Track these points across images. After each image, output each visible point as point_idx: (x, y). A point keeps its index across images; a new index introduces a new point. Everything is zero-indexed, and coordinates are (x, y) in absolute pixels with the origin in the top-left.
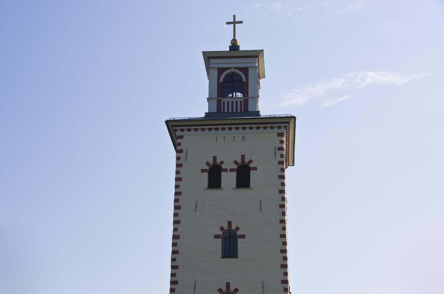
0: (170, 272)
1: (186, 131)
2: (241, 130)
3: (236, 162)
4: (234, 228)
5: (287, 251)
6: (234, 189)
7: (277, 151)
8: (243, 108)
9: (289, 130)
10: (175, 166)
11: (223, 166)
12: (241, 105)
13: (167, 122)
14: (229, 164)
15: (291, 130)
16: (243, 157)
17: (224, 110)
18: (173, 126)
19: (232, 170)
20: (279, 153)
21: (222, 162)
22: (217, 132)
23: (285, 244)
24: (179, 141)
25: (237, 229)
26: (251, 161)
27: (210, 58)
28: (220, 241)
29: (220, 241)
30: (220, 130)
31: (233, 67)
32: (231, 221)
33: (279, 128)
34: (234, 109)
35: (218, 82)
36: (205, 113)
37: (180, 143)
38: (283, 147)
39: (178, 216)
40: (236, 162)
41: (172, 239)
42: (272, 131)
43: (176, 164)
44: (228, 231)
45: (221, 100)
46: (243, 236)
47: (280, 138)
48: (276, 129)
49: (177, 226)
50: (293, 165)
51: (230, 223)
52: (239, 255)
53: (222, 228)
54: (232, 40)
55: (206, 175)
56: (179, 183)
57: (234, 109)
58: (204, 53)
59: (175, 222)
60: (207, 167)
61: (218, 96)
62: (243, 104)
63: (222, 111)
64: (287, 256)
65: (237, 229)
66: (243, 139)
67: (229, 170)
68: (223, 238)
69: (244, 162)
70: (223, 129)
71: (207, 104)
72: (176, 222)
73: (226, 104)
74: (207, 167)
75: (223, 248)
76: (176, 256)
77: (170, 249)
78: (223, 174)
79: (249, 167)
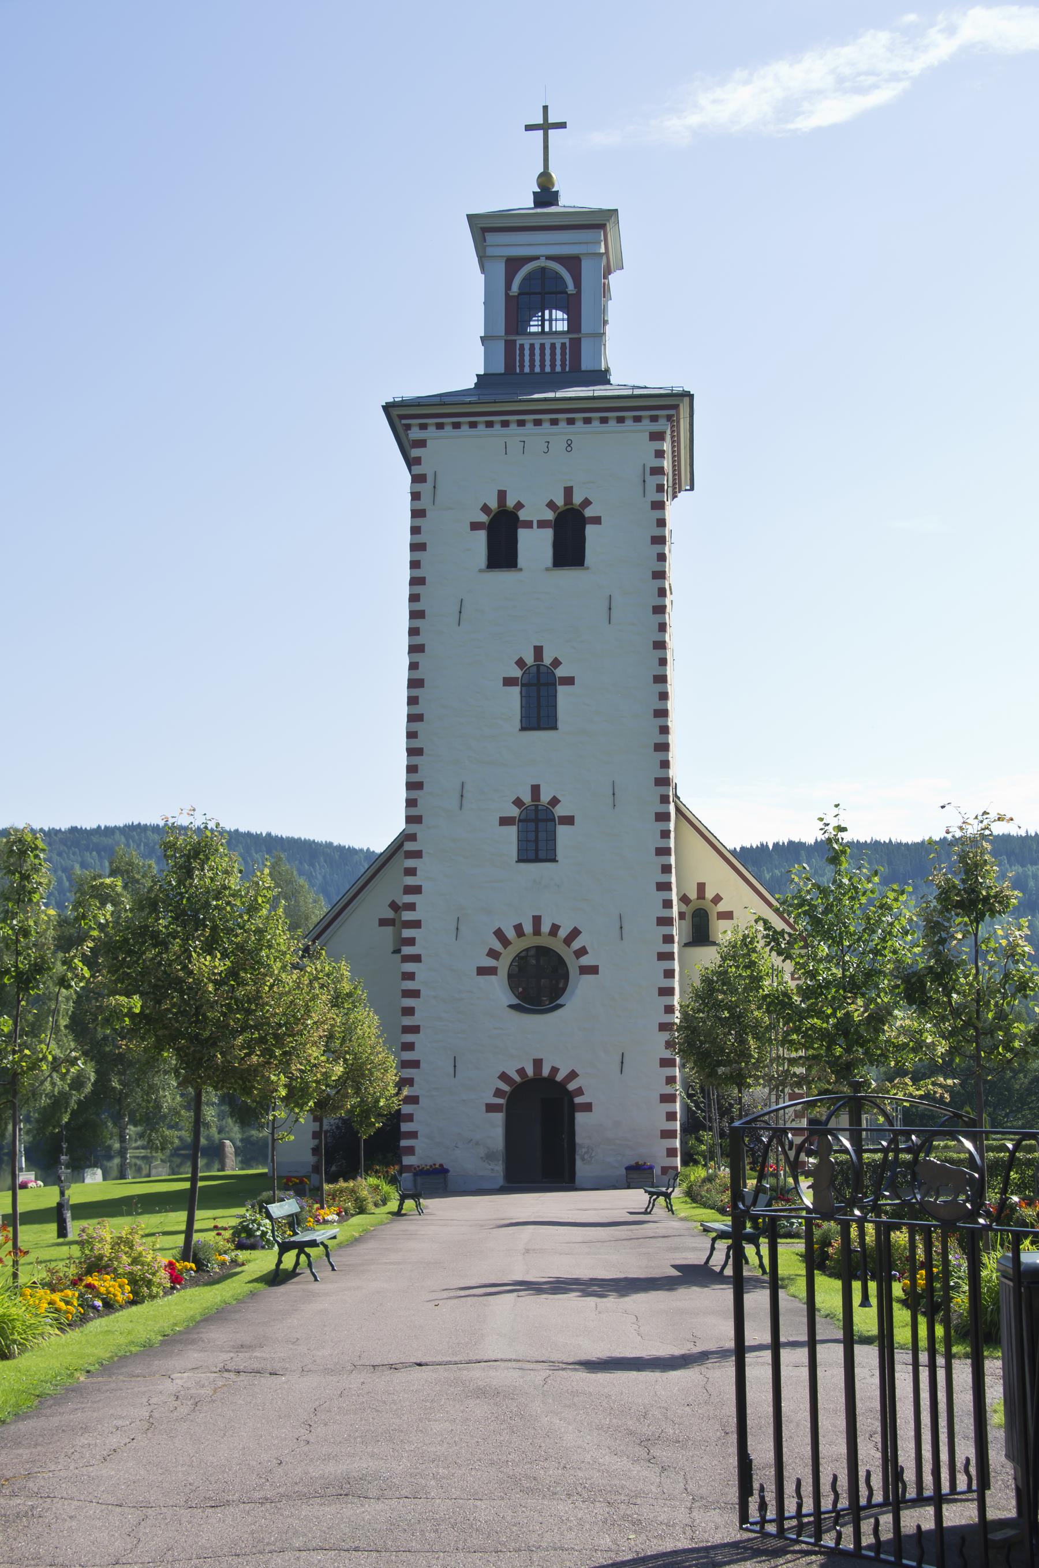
0: (405, 763)
1: (432, 429)
2: (563, 424)
3: (551, 505)
4: (547, 660)
5: (670, 713)
6: (547, 569)
7: (648, 477)
8: (567, 363)
9: (678, 422)
10: (406, 649)
11: (523, 515)
12: (563, 354)
13: (388, 408)
14: (536, 509)
15: (682, 421)
16: (568, 491)
17: (522, 366)
18: (402, 417)
19: (542, 524)
20: (653, 481)
21: (519, 506)
22: (505, 431)
23: (664, 696)
24: (415, 453)
25: (556, 663)
26: (587, 503)
27: (485, 230)
28: (516, 691)
29: (516, 691)
30: (513, 426)
31: (543, 256)
32: (542, 647)
33: (654, 419)
34: (548, 363)
35: (507, 295)
36: (477, 375)
37: (420, 458)
38: (663, 468)
39: (418, 600)
40: (551, 505)
41: (408, 687)
42: (638, 426)
43: (412, 510)
44: (534, 669)
45: (515, 341)
46: (569, 681)
47: (656, 445)
48: (646, 422)
49: (418, 657)
50: (692, 489)
51: (538, 651)
52: (560, 724)
53: (520, 663)
54: (541, 175)
55: (482, 535)
56: (419, 555)
57: (548, 363)
58: (470, 218)
59: (414, 649)
60: (484, 518)
61: (507, 332)
62: (568, 351)
63: (518, 371)
64: (670, 759)
65: (556, 663)
66: (569, 449)
67: (535, 525)
68: (523, 685)
69: (572, 504)
70: (521, 423)
71: (481, 350)
72: (414, 649)
73: (527, 352)
74: (484, 518)
75: (524, 719)
76: (416, 726)
77: (402, 710)
78: (522, 534)
79: (583, 516)
